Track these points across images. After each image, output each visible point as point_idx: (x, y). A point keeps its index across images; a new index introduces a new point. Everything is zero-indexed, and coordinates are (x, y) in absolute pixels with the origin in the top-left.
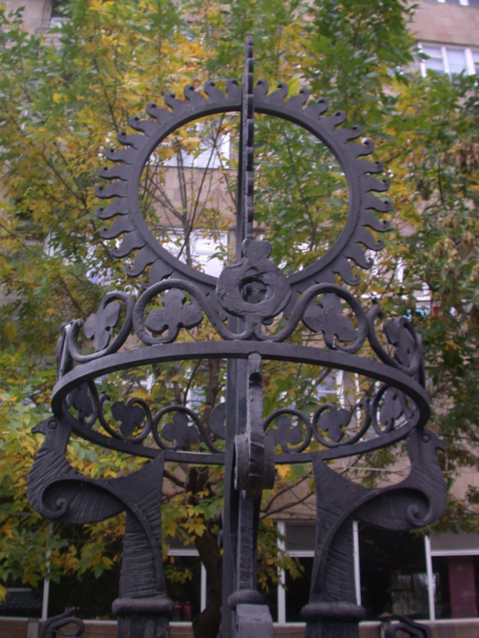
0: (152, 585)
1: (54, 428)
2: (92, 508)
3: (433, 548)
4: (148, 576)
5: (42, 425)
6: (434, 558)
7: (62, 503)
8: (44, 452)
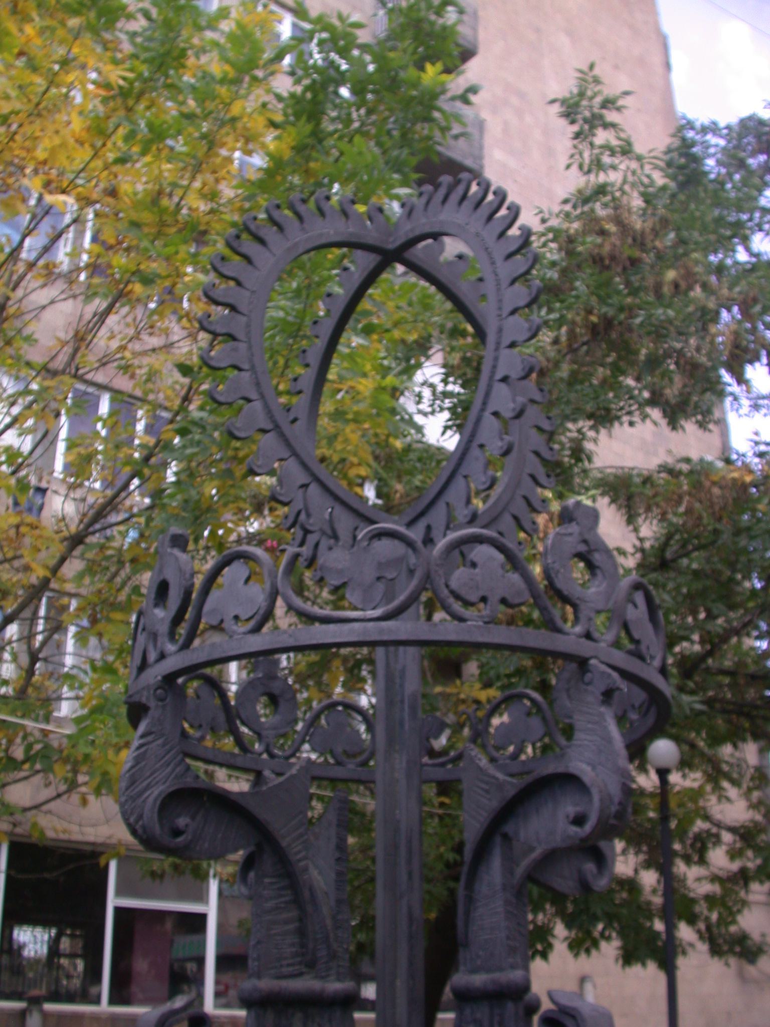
0: (299, 959)
1: (162, 700)
2: (220, 836)
3: (119, 893)
4: (293, 945)
5: (145, 693)
6: (118, 910)
7: (187, 825)
8: (150, 738)
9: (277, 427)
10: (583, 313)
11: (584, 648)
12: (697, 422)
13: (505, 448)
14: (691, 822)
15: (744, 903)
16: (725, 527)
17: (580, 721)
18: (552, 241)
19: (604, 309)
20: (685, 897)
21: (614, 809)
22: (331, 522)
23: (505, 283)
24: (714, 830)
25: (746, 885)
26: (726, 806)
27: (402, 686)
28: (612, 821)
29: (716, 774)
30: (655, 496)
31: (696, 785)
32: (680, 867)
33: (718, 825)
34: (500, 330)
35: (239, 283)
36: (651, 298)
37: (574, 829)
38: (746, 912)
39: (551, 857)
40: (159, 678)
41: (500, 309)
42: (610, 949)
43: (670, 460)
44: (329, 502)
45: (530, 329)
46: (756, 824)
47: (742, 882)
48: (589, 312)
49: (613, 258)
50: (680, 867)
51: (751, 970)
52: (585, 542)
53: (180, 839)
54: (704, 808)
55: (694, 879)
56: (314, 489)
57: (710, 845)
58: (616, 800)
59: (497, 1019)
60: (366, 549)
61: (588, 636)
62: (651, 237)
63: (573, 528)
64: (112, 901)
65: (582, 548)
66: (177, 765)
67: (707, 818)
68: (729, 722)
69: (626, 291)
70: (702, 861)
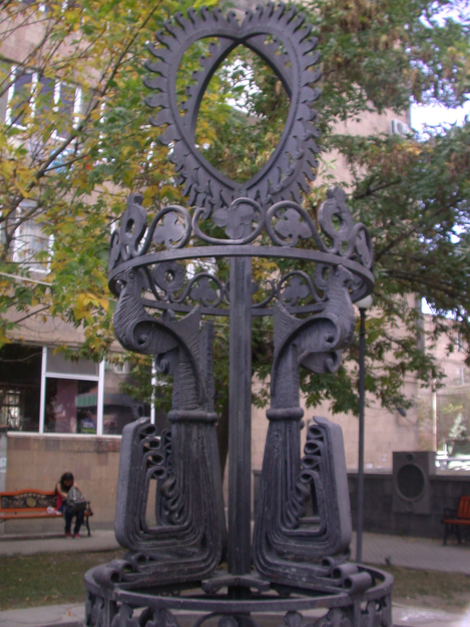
0: (195, 401)
3: (48, 370)
4: (193, 394)
6: (48, 380)
8: (128, 297)
9: (183, 139)
10: (333, 56)
11: (336, 260)
12: (393, 110)
13: (300, 155)
14: (376, 337)
15: (401, 383)
16: (404, 176)
17: (331, 294)
18: (317, 7)
19: (345, 55)
20: (369, 377)
21: (347, 335)
22: (209, 187)
23: (303, 68)
24: (388, 341)
25: (403, 372)
26: (396, 330)
27: (243, 271)
28: (346, 341)
29: (390, 310)
30: (366, 156)
31: (379, 317)
32: (369, 361)
33: (390, 339)
34: (299, 94)
35: (163, 60)
36: (371, 50)
37: (328, 344)
38: (401, 387)
39: (311, 356)
40: (131, 268)
41: (300, 82)
42: (327, 403)
43: (375, 134)
44: (209, 178)
45: (315, 95)
46: (411, 339)
47: (401, 371)
48: (337, 55)
49: (353, 23)
50: (369, 361)
51: (403, 420)
52: (339, 208)
53: (143, 345)
54: (384, 330)
55: (377, 368)
56: (201, 171)
57: (385, 349)
58: (348, 331)
59: (288, 429)
60: (235, 210)
61: (338, 254)
62: (375, 13)
63: (333, 201)
64: (45, 374)
65: (337, 211)
66: (140, 310)
67: (384, 335)
68: (399, 282)
69: (358, 44)
70: (380, 357)
